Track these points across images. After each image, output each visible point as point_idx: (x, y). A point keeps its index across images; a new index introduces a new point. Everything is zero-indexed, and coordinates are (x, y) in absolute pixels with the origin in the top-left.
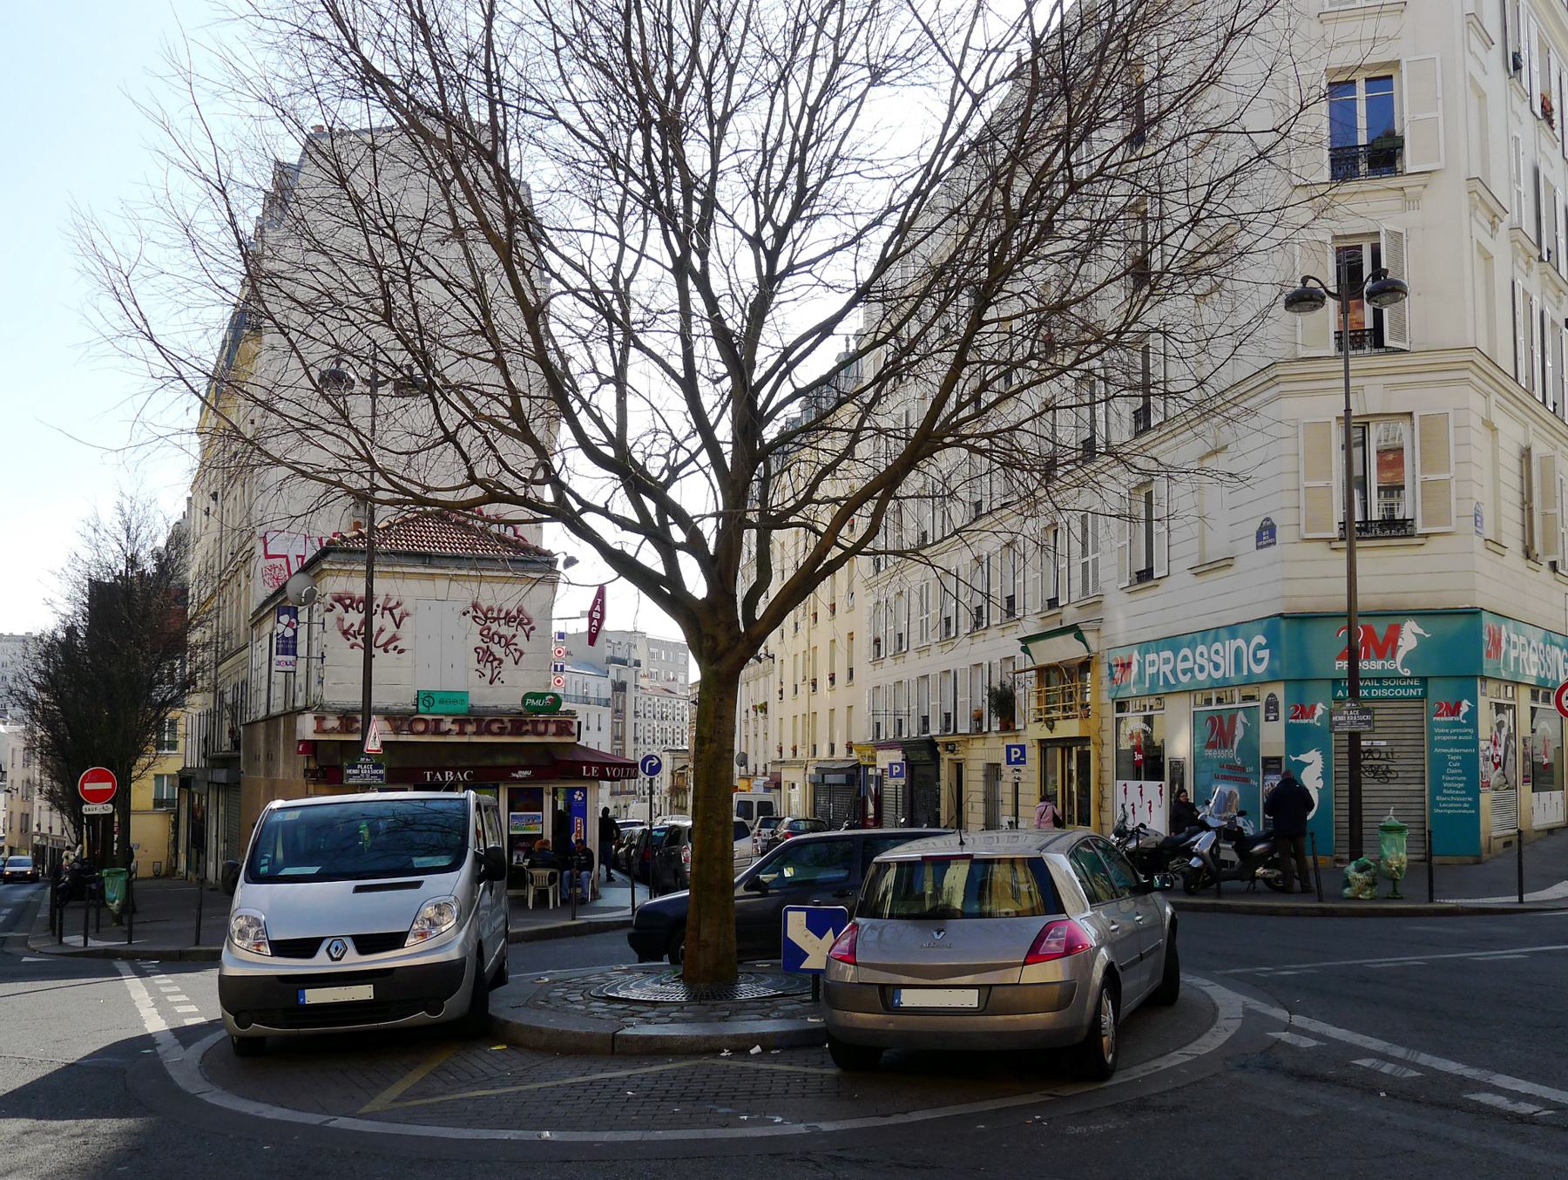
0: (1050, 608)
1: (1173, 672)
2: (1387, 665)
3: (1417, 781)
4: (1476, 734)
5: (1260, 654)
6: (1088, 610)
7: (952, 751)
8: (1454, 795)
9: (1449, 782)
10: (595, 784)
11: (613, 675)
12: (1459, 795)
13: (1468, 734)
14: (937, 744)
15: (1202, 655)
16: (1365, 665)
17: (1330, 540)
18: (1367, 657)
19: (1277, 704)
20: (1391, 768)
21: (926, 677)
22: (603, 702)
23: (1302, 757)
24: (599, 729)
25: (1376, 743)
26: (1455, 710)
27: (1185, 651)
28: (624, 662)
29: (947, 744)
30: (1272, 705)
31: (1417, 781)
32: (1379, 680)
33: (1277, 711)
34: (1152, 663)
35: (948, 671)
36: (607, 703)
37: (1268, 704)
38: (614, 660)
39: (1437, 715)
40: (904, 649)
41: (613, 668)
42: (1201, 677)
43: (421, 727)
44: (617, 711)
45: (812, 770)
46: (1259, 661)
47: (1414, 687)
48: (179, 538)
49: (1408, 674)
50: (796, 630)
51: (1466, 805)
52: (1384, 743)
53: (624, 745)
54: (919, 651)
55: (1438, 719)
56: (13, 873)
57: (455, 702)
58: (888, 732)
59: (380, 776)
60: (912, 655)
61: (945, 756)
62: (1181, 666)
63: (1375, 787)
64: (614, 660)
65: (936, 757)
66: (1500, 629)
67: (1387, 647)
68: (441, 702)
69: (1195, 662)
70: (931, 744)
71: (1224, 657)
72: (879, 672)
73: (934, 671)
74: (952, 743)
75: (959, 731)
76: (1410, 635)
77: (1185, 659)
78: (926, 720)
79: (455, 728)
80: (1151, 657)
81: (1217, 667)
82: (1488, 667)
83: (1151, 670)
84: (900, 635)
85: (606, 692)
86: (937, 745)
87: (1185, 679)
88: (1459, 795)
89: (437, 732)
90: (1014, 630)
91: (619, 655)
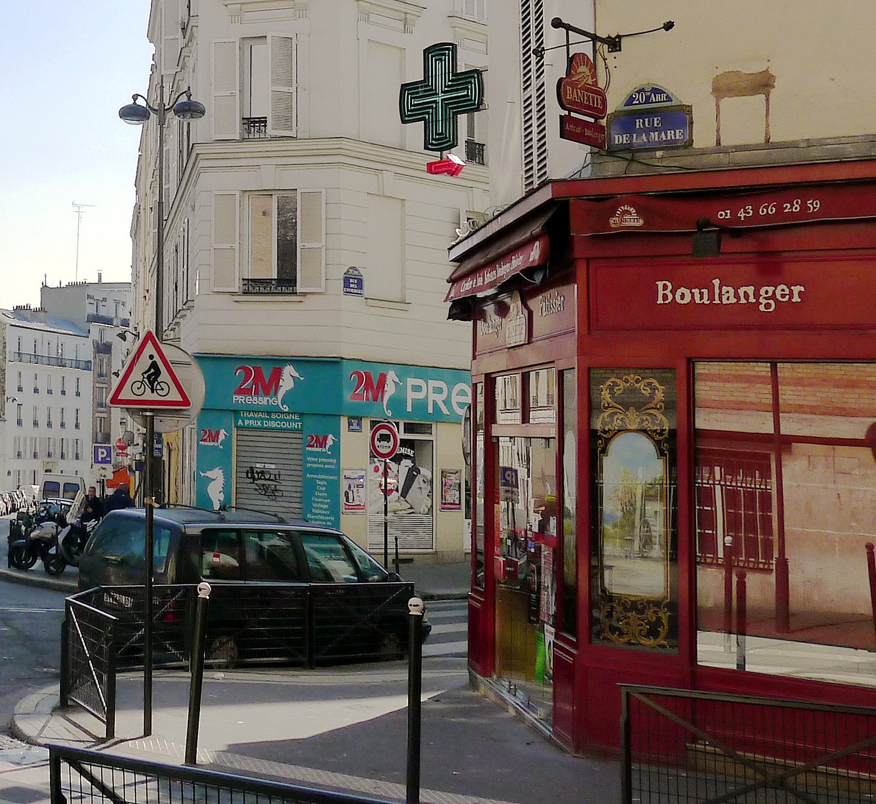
1: (447, 402)
3: (297, 500)
4: (338, 464)
8: (321, 514)
9: (317, 502)
11: (95, 334)
12: (324, 515)
13: (332, 464)
17: (233, 294)
20: (278, 488)
22: (82, 365)
23: (209, 474)
24: (78, 394)
25: (267, 466)
26: (322, 443)
28: (108, 321)
31: (297, 500)
32: (269, 413)
36: (87, 366)
38: (96, 319)
39: (309, 446)
41: (95, 328)
44: (101, 375)
47: (295, 421)
49: (286, 410)
51: (329, 523)
52: (273, 466)
55: (310, 449)
56: (708, 496)
63: (265, 503)
64: (96, 319)
67: (270, 385)
76: (289, 377)
85: (87, 352)
88: (324, 515)
91: (103, 312)
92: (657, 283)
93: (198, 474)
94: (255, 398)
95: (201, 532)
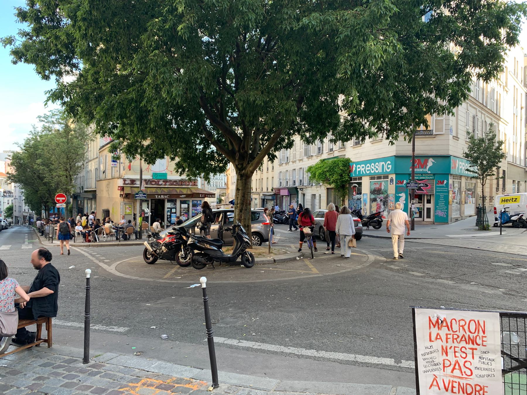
1: (365, 170)
2: (424, 170)
5: (389, 166)
6: (341, 152)
14: (298, 188)
15: (373, 166)
16: (415, 170)
18: (419, 168)
19: (393, 180)
21: (295, 169)
23: (400, 195)
27: (368, 165)
29: (301, 189)
30: (392, 180)
32: (422, 174)
33: (393, 182)
34: (359, 168)
37: (391, 180)
42: (372, 172)
43: (154, 183)
45: (261, 195)
46: (388, 168)
47: (431, 176)
48: (309, 228)
50: (268, 170)
53: (205, 186)
54: (293, 162)
57: (164, 176)
58: (284, 185)
59: (145, 197)
60: (291, 163)
61: (300, 192)
62: (367, 169)
65: (298, 192)
66: (456, 161)
67: (424, 166)
68: (160, 176)
73: (297, 168)
74: (302, 188)
75: (304, 185)
76: (430, 163)
77: (368, 167)
78: (294, 182)
79: (164, 183)
80: (358, 166)
81: (377, 169)
82: (452, 171)
83: (358, 170)
84: (288, 157)
87: (368, 172)
92: (231, 167)
93: (396, 195)
94: (418, 169)
95: (477, 225)
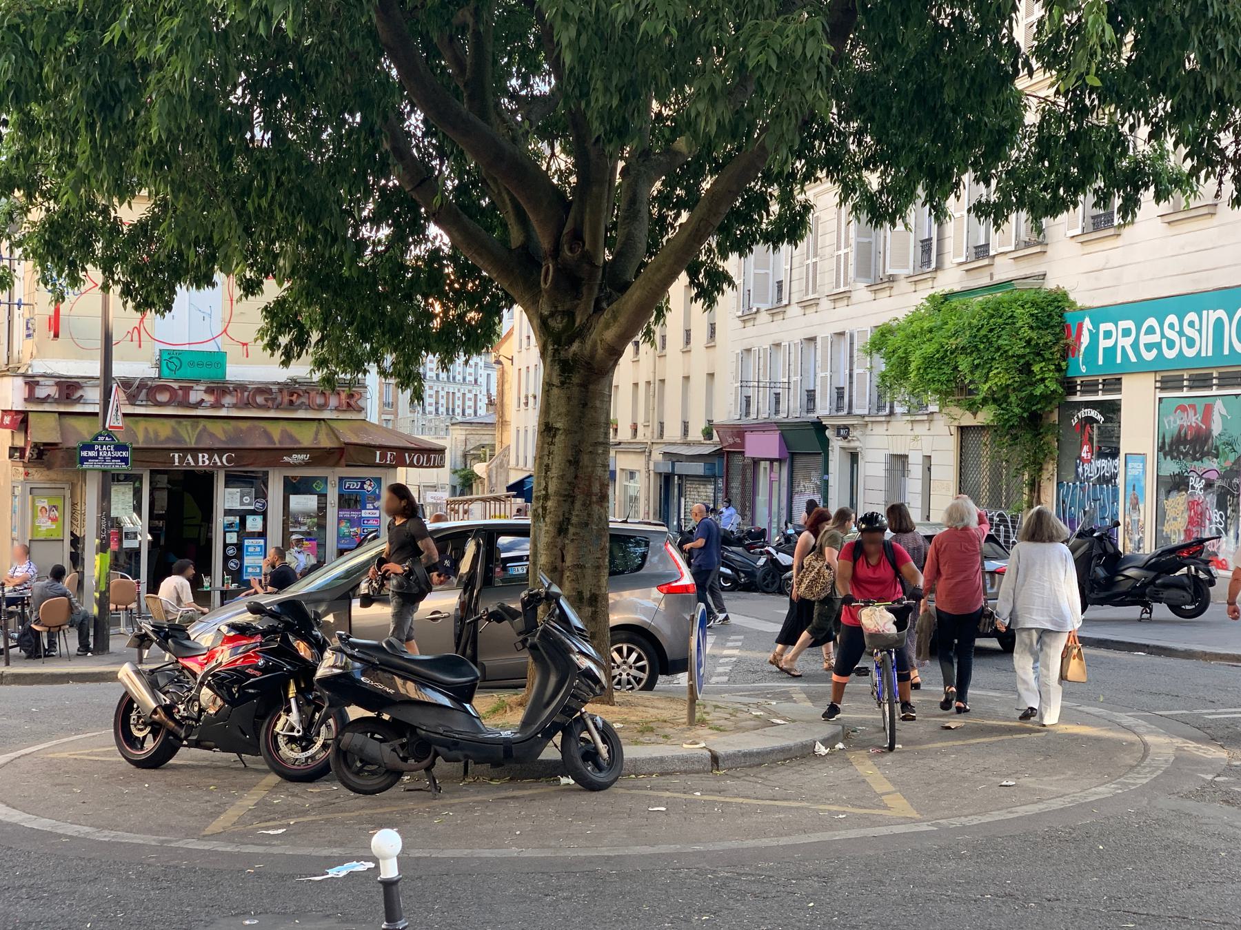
0: (978, 258)
1: (1135, 346)
7: (845, 438)
10: (391, 470)
15: (1171, 326)
21: (812, 339)
29: (839, 428)
34: (1108, 335)
35: (842, 334)
40: (785, 302)
42: (1170, 354)
50: (688, 342)
58: (762, 409)
60: (794, 310)
61: (836, 444)
62: (1144, 339)
65: (825, 443)
68: (191, 364)
69: (1163, 336)
70: (819, 427)
71: (1200, 331)
72: (750, 330)
73: (824, 332)
74: (846, 427)
77: (1151, 330)
78: (811, 395)
79: (209, 399)
80: (1104, 327)
81: (1191, 343)
83: (1104, 344)
86: (825, 427)
87: (1149, 356)
89: (186, 404)
90: (930, 284)
